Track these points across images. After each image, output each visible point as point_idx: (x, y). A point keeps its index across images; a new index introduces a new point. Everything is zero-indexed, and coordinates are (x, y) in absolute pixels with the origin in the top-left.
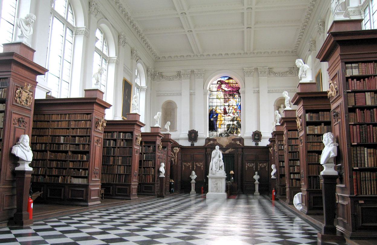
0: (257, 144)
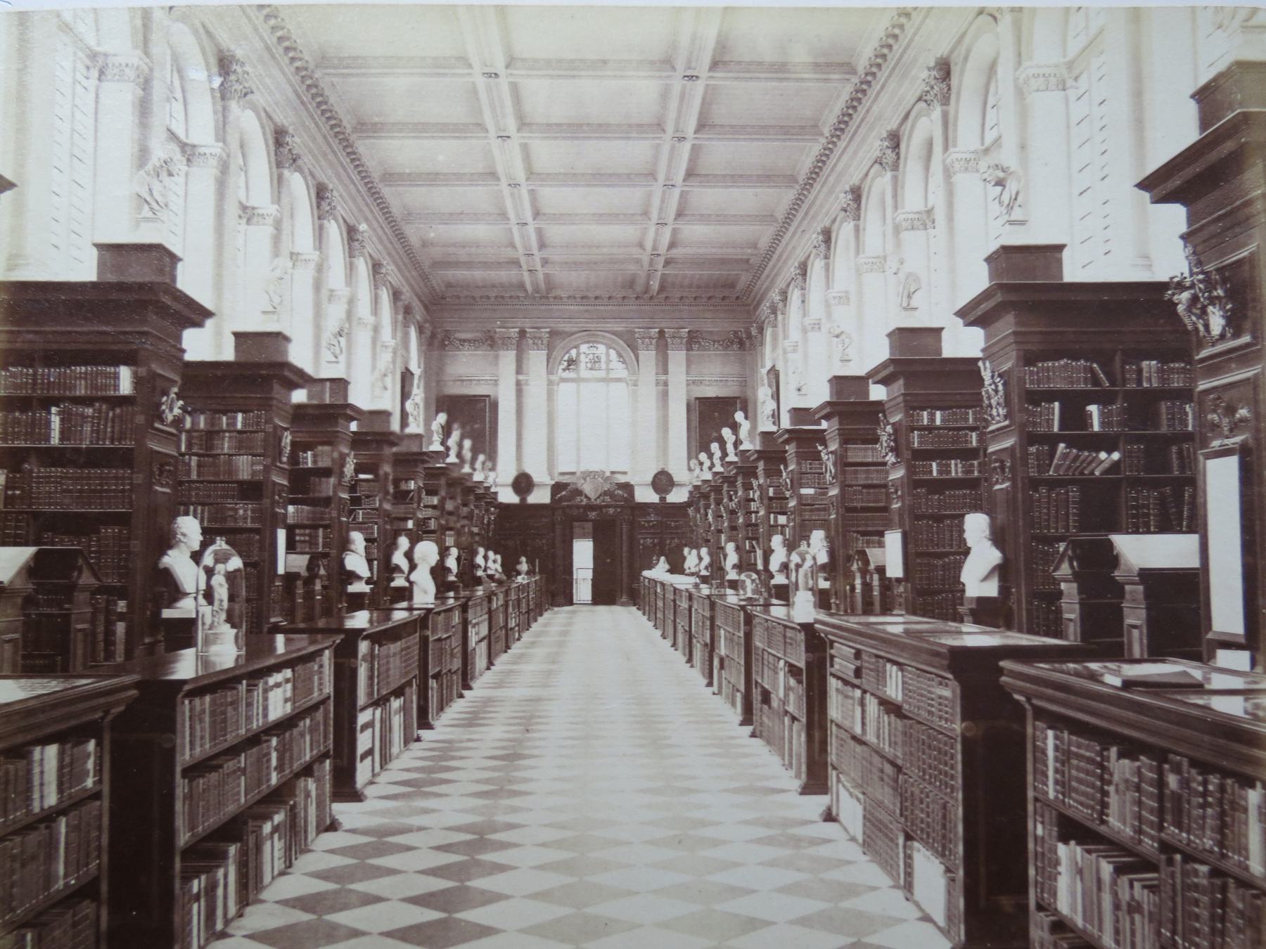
0: (523, 500)
